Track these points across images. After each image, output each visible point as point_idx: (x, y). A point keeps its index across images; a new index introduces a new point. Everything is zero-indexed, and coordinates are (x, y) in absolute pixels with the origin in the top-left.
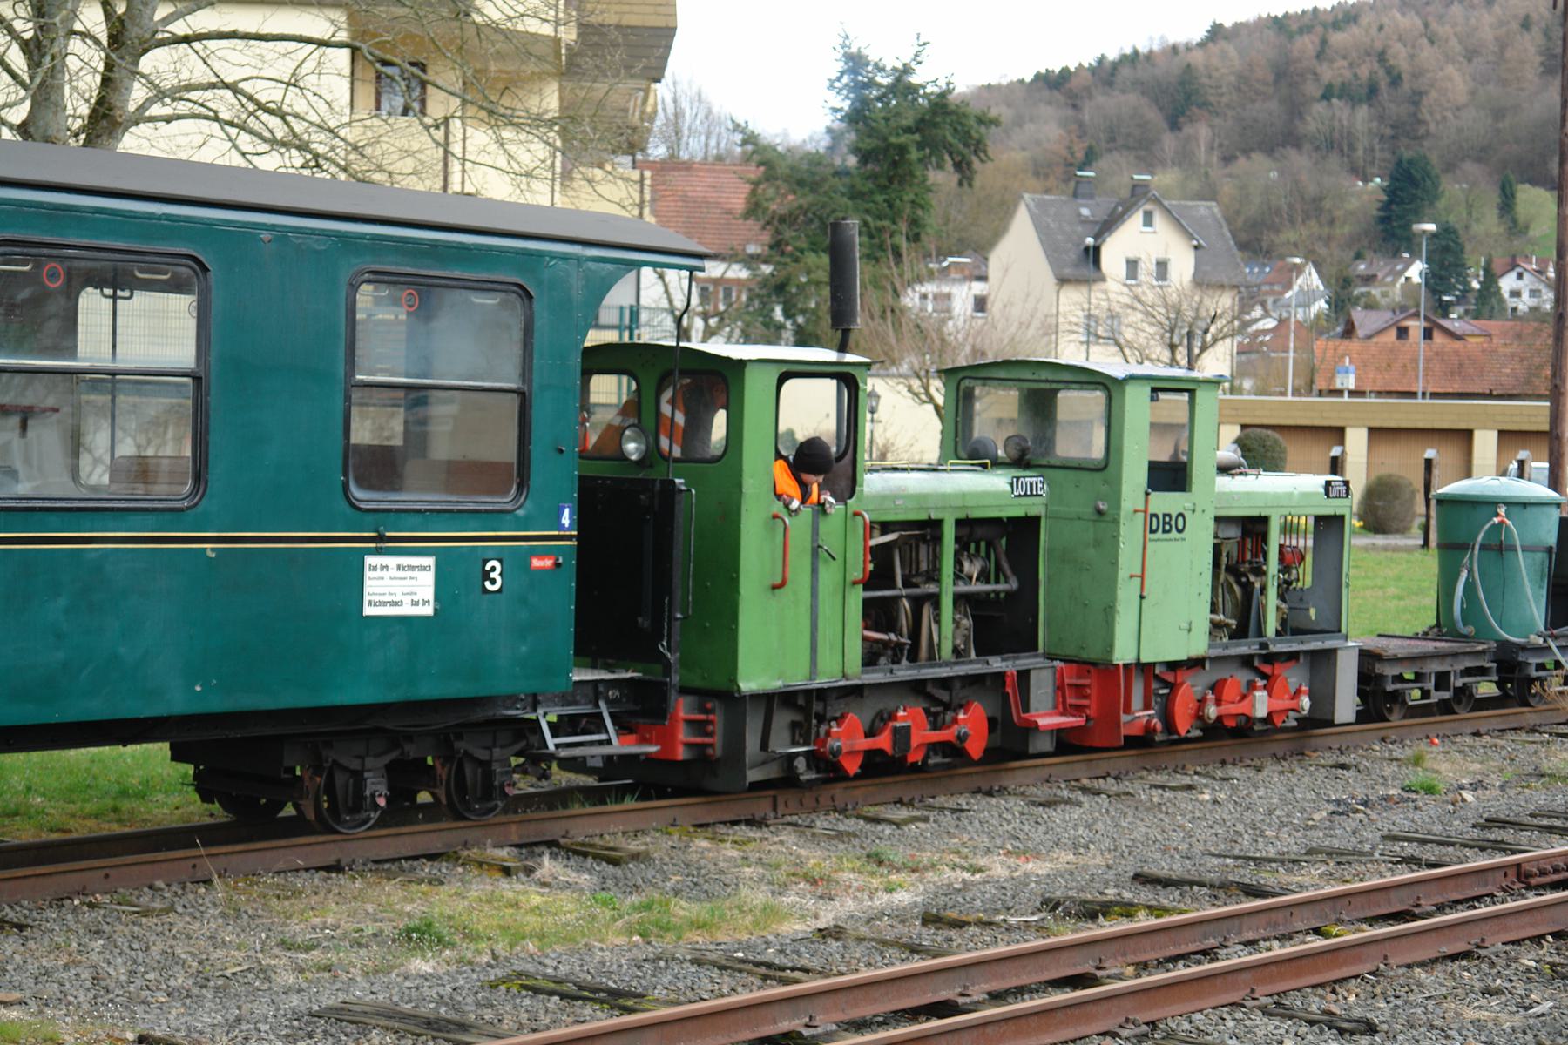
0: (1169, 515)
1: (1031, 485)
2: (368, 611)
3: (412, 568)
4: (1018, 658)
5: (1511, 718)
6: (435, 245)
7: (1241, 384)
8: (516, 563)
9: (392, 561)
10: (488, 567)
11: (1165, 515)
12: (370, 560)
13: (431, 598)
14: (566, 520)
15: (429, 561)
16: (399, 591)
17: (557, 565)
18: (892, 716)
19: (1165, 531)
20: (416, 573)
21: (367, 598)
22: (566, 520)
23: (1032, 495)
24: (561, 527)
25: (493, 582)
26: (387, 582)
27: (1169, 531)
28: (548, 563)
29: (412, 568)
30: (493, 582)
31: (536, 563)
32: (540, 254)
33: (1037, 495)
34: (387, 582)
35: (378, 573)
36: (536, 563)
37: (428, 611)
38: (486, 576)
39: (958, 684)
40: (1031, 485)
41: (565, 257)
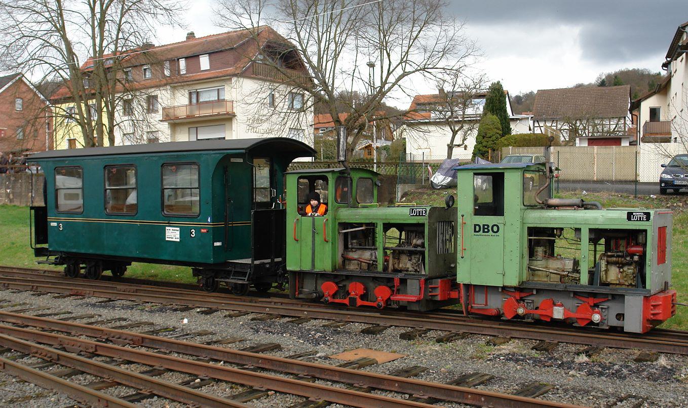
0: (488, 226)
1: (419, 212)
2: (167, 239)
3: (175, 230)
4: (131, 286)
5: (563, 337)
6: (177, 156)
7: (482, 183)
8: (198, 230)
9: (171, 228)
10: (192, 231)
11: (484, 225)
12: (167, 228)
13: (179, 237)
14: (209, 220)
15: (178, 229)
16: (173, 235)
17: (207, 232)
18: (287, 282)
19: (484, 232)
20: (176, 231)
21: (166, 236)
22: (209, 220)
23: (419, 215)
24: (208, 222)
25: (193, 235)
26: (170, 233)
27: (488, 231)
28: (205, 231)
29: (175, 230)
30: (193, 235)
31: (202, 231)
32: (201, 154)
33: (422, 215)
34: (170, 233)
35: (168, 231)
36: (202, 231)
37: (178, 240)
38: (191, 233)
39: (319, 275)
40: (419, 212)
41: (207, 154)
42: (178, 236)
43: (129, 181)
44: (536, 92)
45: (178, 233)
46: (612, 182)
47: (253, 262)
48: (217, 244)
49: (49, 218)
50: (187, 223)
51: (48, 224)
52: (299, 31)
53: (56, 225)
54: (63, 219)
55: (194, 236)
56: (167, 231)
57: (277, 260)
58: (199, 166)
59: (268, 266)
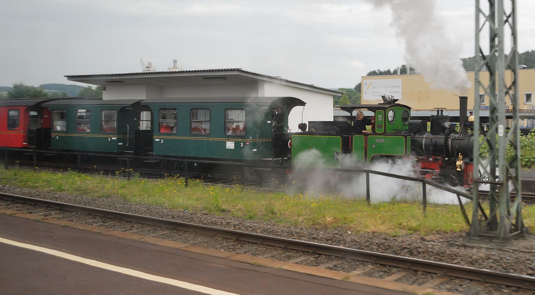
2: (227, 148)
12: (227, 142)
15: (234, 142)
21: (227, 146)
22: (251, 138)
24: (250, 139)
37: (233, 148)
38: (241, 145)
42: (234, 146)
43: (228, 117)
44: (530, 51)
45: (234, 144)
46: (281, 80)
47: (273, 159)
48: (254, 150)
49: (154, 137)
50: (239, 140)
51: (154, 140)
52: (461, 197)
53: (270, 122)
54: (163, 137)
55: (242, 146)
56: (227, 144)
57: (285, 158)
58: (210, 111)
59: (280, 161)
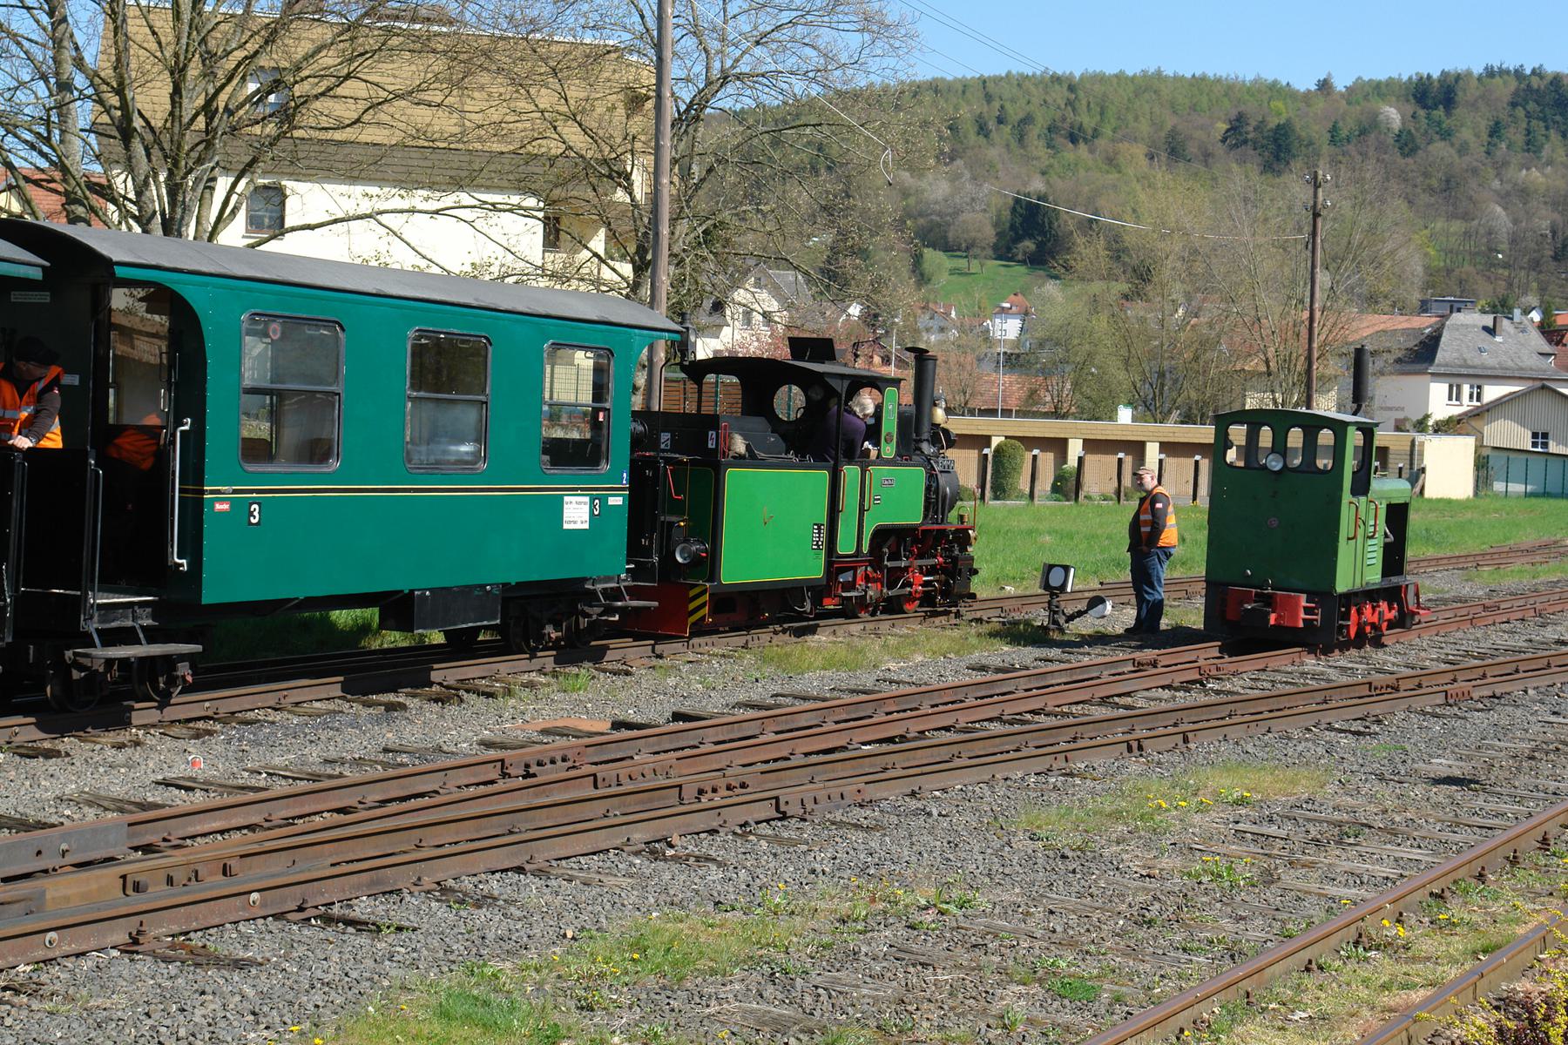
12: (566, 499)
37: (586, 526)
